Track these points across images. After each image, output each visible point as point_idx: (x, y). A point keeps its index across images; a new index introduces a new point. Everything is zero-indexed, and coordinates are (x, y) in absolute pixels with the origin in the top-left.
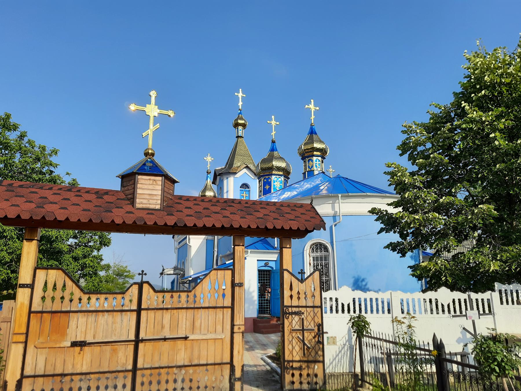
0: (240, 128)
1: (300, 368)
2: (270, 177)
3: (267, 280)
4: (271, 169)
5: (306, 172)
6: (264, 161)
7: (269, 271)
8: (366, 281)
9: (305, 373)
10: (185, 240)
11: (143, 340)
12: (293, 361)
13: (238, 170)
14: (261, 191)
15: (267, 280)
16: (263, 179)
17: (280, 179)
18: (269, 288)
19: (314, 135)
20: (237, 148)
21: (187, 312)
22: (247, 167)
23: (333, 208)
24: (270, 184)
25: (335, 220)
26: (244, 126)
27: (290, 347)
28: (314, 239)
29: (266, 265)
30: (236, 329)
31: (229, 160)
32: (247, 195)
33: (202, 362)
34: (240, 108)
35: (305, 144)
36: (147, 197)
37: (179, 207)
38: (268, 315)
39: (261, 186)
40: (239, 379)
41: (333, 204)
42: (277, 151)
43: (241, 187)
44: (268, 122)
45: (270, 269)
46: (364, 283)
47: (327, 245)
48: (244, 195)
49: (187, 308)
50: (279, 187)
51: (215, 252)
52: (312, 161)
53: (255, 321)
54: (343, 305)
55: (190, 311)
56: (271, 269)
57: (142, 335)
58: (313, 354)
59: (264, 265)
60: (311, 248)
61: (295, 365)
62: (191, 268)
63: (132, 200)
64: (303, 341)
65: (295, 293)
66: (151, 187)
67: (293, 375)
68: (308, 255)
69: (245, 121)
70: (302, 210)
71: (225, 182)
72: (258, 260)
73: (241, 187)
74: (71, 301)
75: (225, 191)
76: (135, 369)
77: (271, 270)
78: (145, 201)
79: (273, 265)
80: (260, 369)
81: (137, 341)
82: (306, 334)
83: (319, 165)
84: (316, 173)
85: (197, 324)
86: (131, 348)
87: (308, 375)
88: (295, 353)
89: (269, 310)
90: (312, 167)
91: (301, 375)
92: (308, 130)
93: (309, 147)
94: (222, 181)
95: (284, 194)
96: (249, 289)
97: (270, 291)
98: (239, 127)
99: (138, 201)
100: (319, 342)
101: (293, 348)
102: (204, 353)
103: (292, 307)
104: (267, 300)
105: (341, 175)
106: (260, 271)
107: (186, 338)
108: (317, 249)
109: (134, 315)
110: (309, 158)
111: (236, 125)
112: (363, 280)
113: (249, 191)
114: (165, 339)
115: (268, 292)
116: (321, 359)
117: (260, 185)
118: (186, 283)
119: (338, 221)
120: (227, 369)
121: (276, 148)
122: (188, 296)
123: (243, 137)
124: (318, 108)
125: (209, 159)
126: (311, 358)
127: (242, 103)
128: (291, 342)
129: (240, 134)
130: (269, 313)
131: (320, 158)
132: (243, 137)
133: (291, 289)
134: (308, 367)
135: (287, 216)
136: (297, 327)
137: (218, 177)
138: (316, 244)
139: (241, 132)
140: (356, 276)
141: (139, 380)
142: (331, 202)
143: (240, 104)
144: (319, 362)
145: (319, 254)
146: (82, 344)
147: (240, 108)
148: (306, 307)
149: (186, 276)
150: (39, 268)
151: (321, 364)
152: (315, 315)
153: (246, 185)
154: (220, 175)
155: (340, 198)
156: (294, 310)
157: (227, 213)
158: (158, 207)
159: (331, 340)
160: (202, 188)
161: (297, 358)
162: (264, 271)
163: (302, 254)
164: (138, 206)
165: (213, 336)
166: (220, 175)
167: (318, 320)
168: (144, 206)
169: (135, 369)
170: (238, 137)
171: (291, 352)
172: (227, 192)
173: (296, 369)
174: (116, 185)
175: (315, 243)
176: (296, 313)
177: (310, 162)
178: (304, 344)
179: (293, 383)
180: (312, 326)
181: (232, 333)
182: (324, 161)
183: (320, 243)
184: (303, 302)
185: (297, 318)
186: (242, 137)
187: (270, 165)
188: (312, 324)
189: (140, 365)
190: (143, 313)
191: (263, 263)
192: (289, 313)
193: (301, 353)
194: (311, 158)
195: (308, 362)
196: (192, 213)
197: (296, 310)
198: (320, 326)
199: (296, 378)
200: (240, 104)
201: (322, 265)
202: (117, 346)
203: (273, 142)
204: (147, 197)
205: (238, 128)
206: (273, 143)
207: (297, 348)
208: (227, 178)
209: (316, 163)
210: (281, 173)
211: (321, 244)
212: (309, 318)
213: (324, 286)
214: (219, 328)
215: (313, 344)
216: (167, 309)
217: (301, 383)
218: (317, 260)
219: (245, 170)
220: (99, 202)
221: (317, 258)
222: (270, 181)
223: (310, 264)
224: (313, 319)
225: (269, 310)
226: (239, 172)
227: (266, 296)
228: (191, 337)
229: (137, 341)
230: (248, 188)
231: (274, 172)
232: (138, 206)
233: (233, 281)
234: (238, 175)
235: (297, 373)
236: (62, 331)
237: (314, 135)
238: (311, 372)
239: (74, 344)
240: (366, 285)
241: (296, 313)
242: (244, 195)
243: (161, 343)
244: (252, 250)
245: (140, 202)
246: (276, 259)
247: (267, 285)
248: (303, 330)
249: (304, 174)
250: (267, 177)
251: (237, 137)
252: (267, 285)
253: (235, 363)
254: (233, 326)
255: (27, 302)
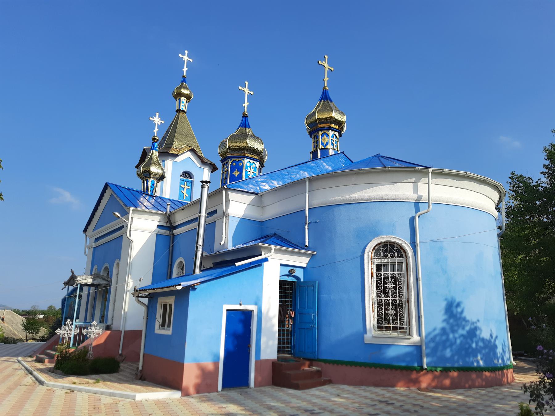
0: (183, 99)
2: (241, 159)
5: (319, 150)
6: (233, 138)
8: (462, 306)
10: (382, 165)
13: (181, 152)
14: (226, 178)
16: (230, 162)
17: (254, 165)
18: (291, 310)
20: (178, 125)
22: (193, 150)
23: (415, 190)
24: (240, 170)
25: (417, 210)
28: (383, 235)
29: (291, 273)
32: (189, 187)
34: (185, 74)
38: (289, 354)
39: (227, 171)
41: (416, 183)
42: (250, 128)
43: (181, 176)
44: (240, 88)
45: (294, 280)
46: (459, 310)
48: (185, 186)
50: (252, 175)
51: (199, 247)
52: (328, 135)
53: (275, 366)
56: (296, 281)
59: (288, 273)
60: (374, 249)
62: (130, 276)
72: (281, 265)
77: (296, 282)
79: (299, 273)
83: (336, 143)
84: (331, 152)
89: (291, 347)
90: (327, 144)
96: (268, 312)
97: (293, 316)
98: (182, 98)
104: (288, 330)
105: (382, 154)
106: (282, 283)
108: (386, 252)
110: (323, 132)
111: (178, 95)
112: (458, 305)
113: (192, 182)
115: (290, 317)
117: (226, 169)
119: (426, 211)
121: (248, 124)
123: (186, 113)
125: (157, 120)
127: (187, 69)
129: (183, 107)
130: (291, 351)
132: (186, 113)
138: (385, 244)
139: (183, 105)
140: (449, 298)
142: (413, 180)
143: (185, 69)
147: (185, 74)
153: (188, 174)
155: (430, 174)
163: (359, 259)
170: (179, 111)
175: (384, 243)
177: (325, 136)
183: (390, 242)
186: (184, 111)
191: (286, 271)
194: (327, 132)
200: (185, 69)
201: (394, 278)
203: (245, 116)
205: (180, 100)
206: (245, 117)
209: (332, 139)
213: (385, 313)
219: (189, 154)
222: (240, 165)
223: (372, 275)
225: (291, 347)
226: (182, 154)
227: (287, 324)
230: (191, 178)
234: (178, 159)
240: (462, 312)
242: (185, 186)
244: (278, 247)
246: (305, 265)
247: (288, 306)
250: (237, 160)
252: (288, 306)
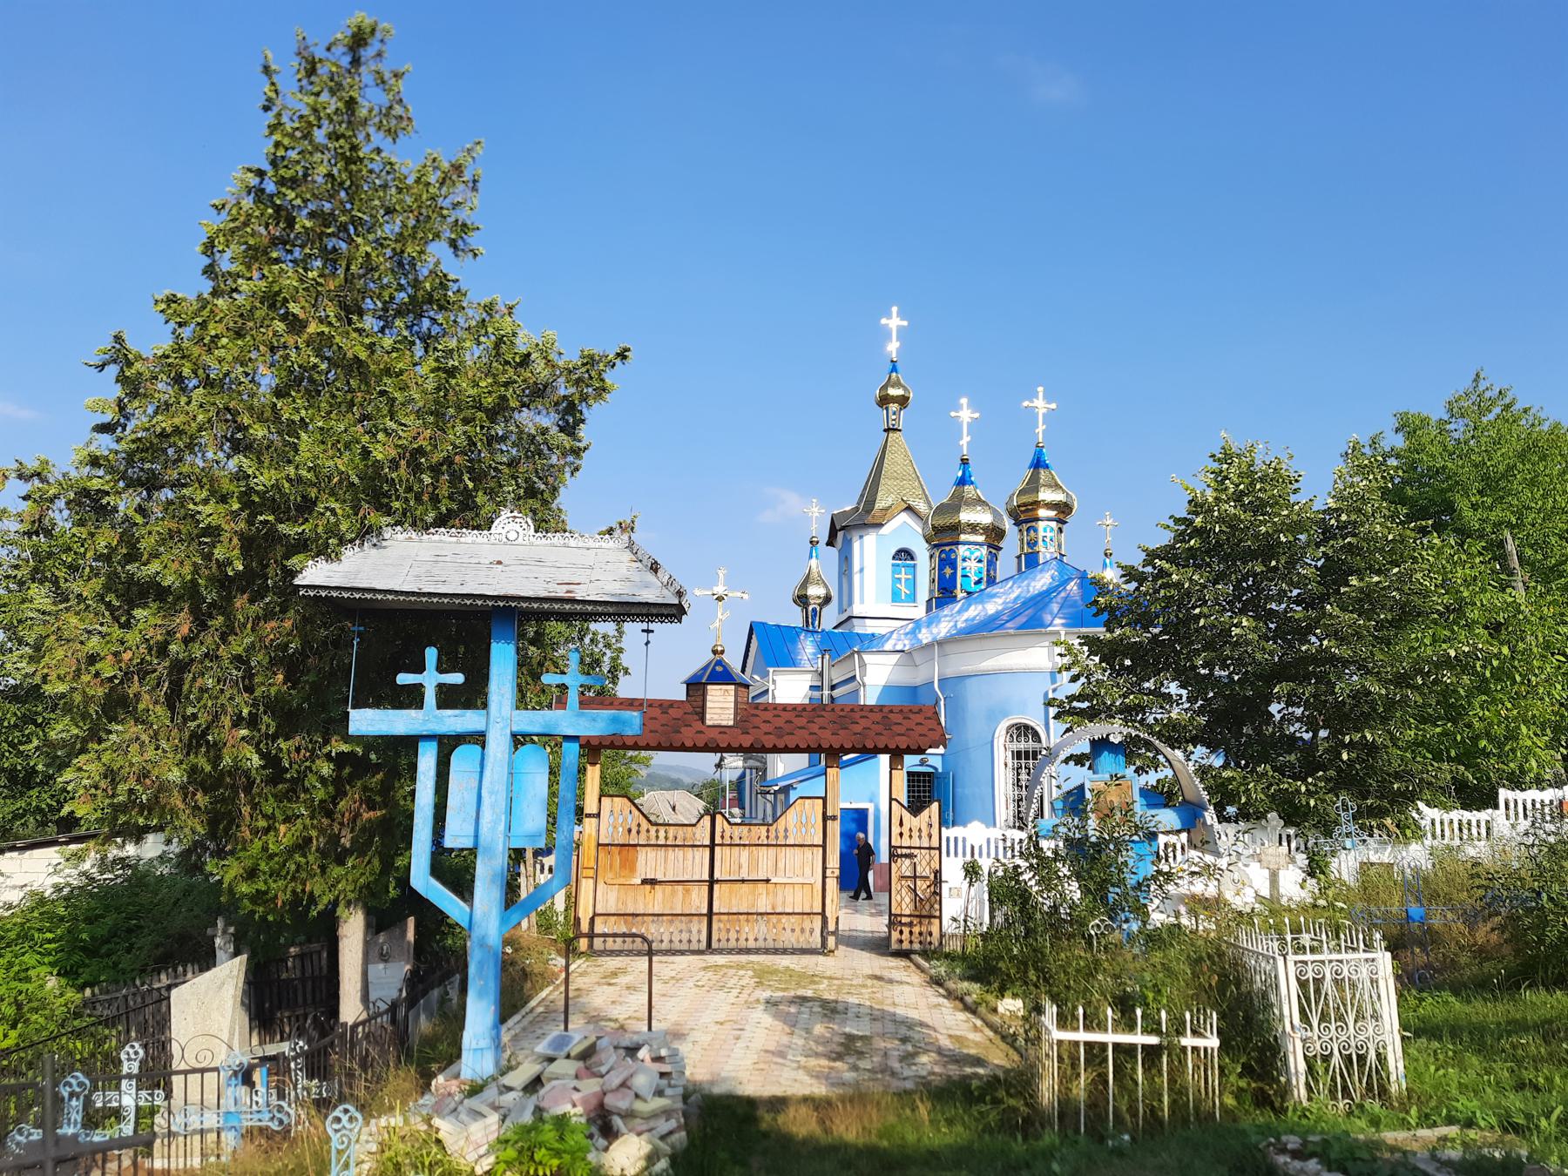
1: (911, 924)
3: (924, 791)
4: (956, 528)
7: (929, 774)
9: (916, 930)
11: (718, 881)
12: (901, 915)
15: (924, 791)
19: (1042, 471)
21: (476, 836)
24: (953, 565)
26: (903, 401)
27: (899, 898)
30: (828, 873)
31: (865, 488)
33: (787, 911)
35: (1022, 492)
36: (719, 711)
37: (756, 721)
40: (833, 933)
45: (931, 770)
47: (1038, 728)
49: (768, 845)
52: (1036, 531)
54: (973, 847)
55: (772, 850)
57: (717, 876)
58: (927, 907)
61: (904, 920)
63: (701, 714)
64: (915, 891)
65: (905, 830)
66: (721, 699)
67: (901, 932)
68: (1002, 749)
69: (905, 389)
70: (918, 718)
71: (856, 545)
73: (894, 558)
74: (638, 832)
75: (856, 567)
76: (710, 914)
78: (716, 717)
80: (876, 935)
81: (712, 882)
82: (919, 882)
85: (781, 865)
86: (705, 889)
87: (921, 934)
88: (904, 906)
91: (911, 933)
92: (1029, 458)
93: (1026, 499)
94: (848, 544)
95: (967, 610)
99: (708, 716)
100: (935, 893)
101: (902, 899)
102: (789, 899)
103: (901, 847)
107: (768, 881)
109: (707, 852)
113: (914, 566)
114: (743, 881)
116: (937, 914)
118: (768, 793)
120: (818, 921)
122: (768, 831)
124: (1053, 406)
126: (924, 913)
128: (899, 892)
131: (1054, 524)
133: (901, 824)
134: (920, 923)
135: (894, 728)
136: (908, 874)
137: (840, 535)
141: (704, 937)
144: (935, 917)
145: (1022, 746)
146: (652, 882)
148: (920, 848)
149: (769, 777)
150: (440, 745)
151: (937, 921)
152: (932, 858)
154: (843, 528)
156: (905, 851)
157: (815, 728)
158: (731, 723)
159: (954, 892)
160: (800, 579)
161: (908, 912)
162: (919, 774)
164: (709, 723)
165: (801, 880)
166: (843, 528)
167: (935, 865)
168: (716, 723)
169: (710, 914)
171: (900, 904)
172: (862, 570)
173: (905, 924)
174: (680, 694)
176: (906, 856)
178: (916, 895)
179: (901, 941)
180: (927, 872)
181: (824, 877)
182: (1065, 527)
184: (915, 842)
185: (907, 862)
187: (953, 520)
188: (927, 869)
189: (715, 909)
190: (717, 849)
192: (898, 856)
193: (912, 906)
195: (920, 916)
196: (771, 730)
197: (908, 851)
198: (938, 873)
199: (906, 935)
202: (691, 887)
203: (964, 462)
204: (719, 711)
207: (907, 900)
208: (861, 537)
210: (981, 539)
211: (1027, 727)
212: (924, 863)
214: (808, 871)
215: (928, 895)
216: (744, 845)
217: (911, 942)
218: (1019, 757)
220: (664, 719)
221: (1019, 753)
224: (929, 863)
228: (774, 880)
229: (712, 882)
230: (912, 559)
231: (963, 537)
232: (709, 723)
233: (824, 813)
234: (884, 530)
235: (906, 930)
236: (629, 866)
237: (1042, 471)
238: (924, 929)
239: (645, 882)
241: (906, 856)
242: (903, 576)
243: (738, 885)
245: (712, 718)
248: (915, 877)
249: (1019, 557)
250: (947, 548)
251: (887, 430)
253: (828, 914)
254: (824, 869)
255: (594, 834)
